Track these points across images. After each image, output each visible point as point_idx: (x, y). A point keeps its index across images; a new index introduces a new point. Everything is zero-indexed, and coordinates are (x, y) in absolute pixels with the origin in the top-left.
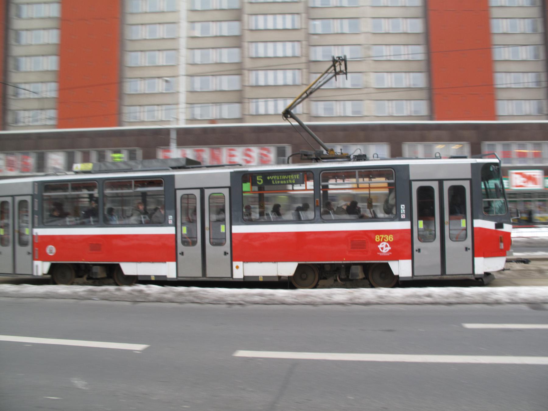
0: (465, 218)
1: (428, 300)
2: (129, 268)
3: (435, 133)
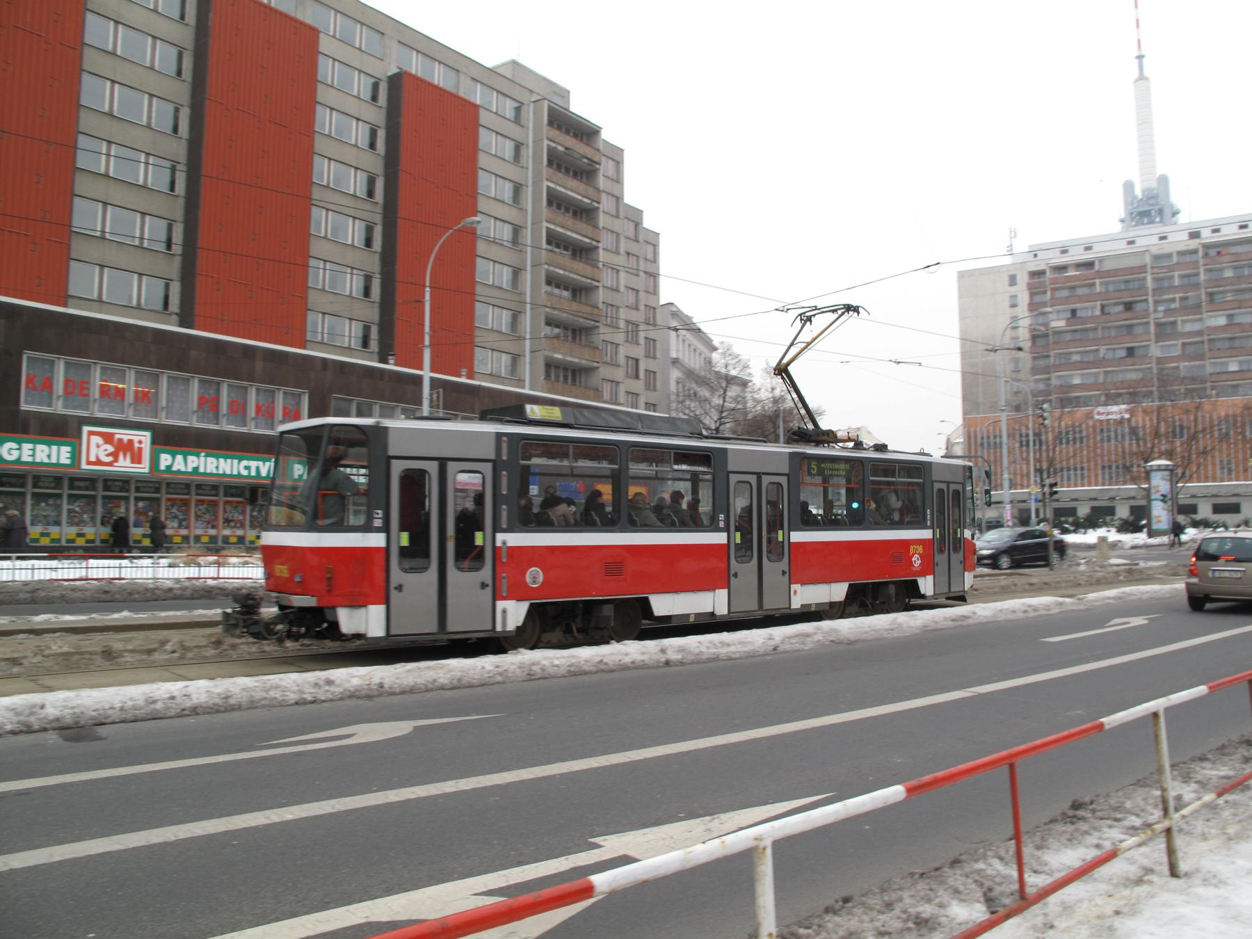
0: (782, 528)
2: (663, 605)
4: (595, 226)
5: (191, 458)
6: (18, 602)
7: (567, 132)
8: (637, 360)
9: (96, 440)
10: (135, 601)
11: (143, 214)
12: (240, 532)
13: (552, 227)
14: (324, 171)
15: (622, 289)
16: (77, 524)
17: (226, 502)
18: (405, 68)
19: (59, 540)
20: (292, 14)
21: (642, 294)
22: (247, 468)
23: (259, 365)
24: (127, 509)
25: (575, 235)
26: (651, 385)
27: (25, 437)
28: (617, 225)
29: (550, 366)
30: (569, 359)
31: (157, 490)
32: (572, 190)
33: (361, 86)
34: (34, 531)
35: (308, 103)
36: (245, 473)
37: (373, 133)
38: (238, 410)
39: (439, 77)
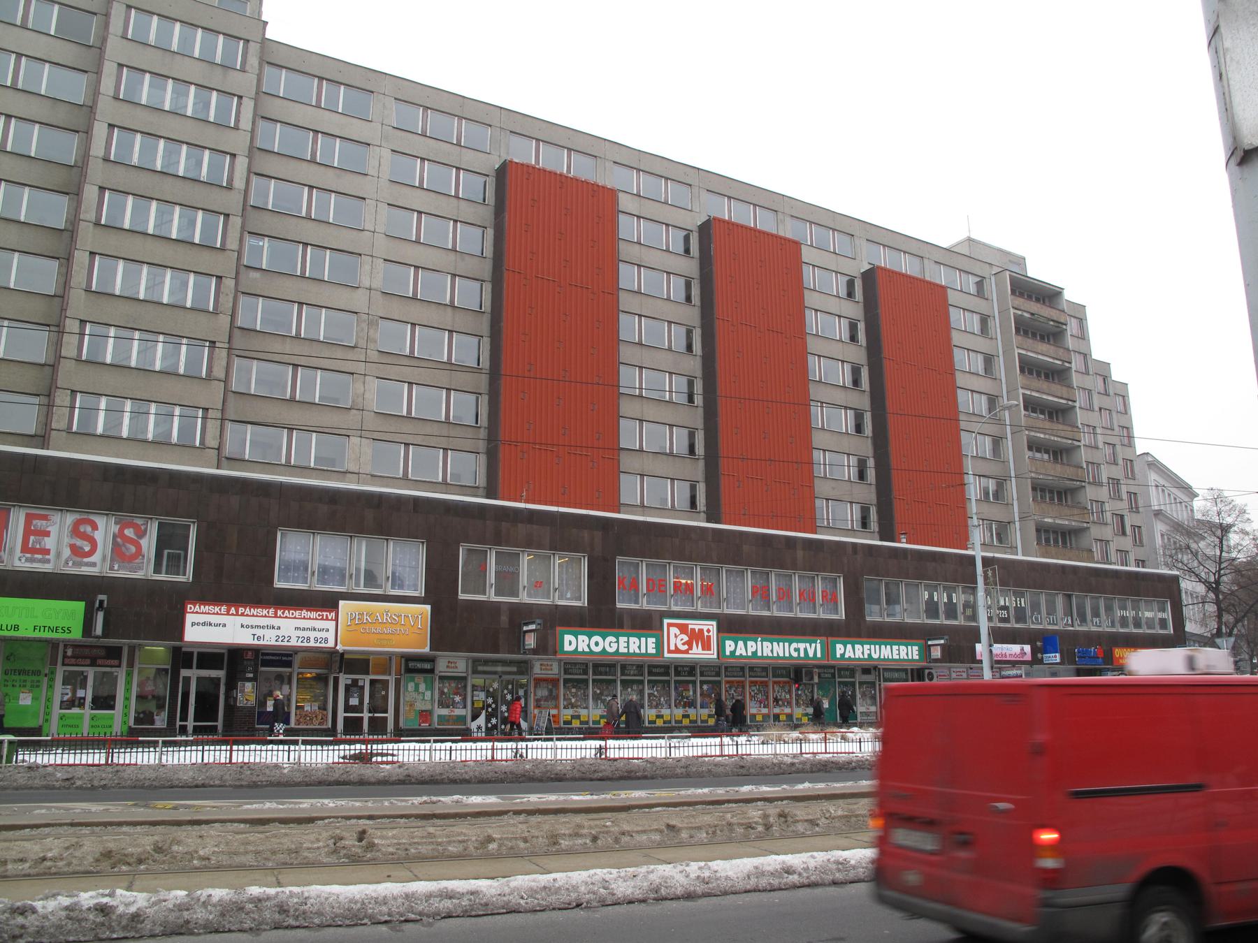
1: (447, 904)
3: (522, 529)
4: (1070, 387)
5: (749, 643)
6: (677, 776)
7: (1030, 298)
8: (1122, 517)
9: (674, 630)
10: (766, 774)
11: (671, 426)
12: (788, 710)
13: (1028, 392)
14: (817, 368)
15: (1101, 445)
16: (656, 707)
17: (775, 683)
18: (877, 263)
19: (587, 723)
20: (774, 232)
21: (1118, 448)
22: (797, 650)
23: (800, 554)
24: (695, 692)
25: (1050, 398)
26: (1138, 542)
27: (621, 631)
28: (1088, 382)
29: (1042, 530)
30: (1058, 521)
31: (718, 674)
32: (1043, 353)
33: (838, 285)
34: (649, 713)
35: (799, 308)
36: (795, 654)
37: (688, 286)
38: (785, 595)
39: (906, 266)
